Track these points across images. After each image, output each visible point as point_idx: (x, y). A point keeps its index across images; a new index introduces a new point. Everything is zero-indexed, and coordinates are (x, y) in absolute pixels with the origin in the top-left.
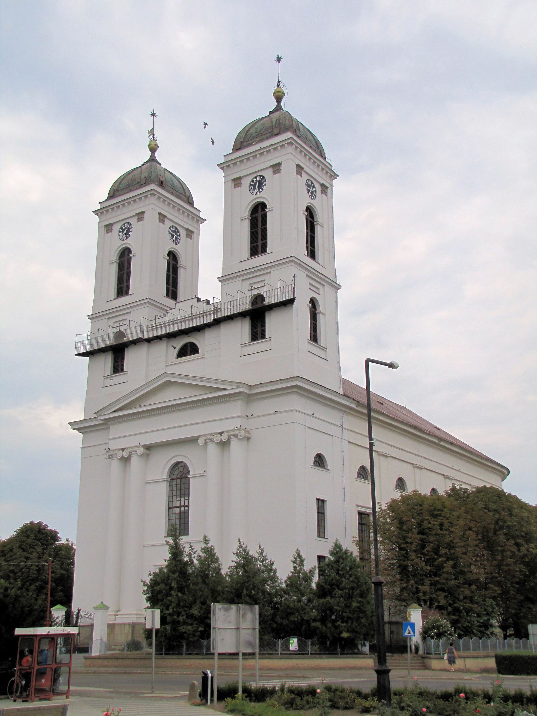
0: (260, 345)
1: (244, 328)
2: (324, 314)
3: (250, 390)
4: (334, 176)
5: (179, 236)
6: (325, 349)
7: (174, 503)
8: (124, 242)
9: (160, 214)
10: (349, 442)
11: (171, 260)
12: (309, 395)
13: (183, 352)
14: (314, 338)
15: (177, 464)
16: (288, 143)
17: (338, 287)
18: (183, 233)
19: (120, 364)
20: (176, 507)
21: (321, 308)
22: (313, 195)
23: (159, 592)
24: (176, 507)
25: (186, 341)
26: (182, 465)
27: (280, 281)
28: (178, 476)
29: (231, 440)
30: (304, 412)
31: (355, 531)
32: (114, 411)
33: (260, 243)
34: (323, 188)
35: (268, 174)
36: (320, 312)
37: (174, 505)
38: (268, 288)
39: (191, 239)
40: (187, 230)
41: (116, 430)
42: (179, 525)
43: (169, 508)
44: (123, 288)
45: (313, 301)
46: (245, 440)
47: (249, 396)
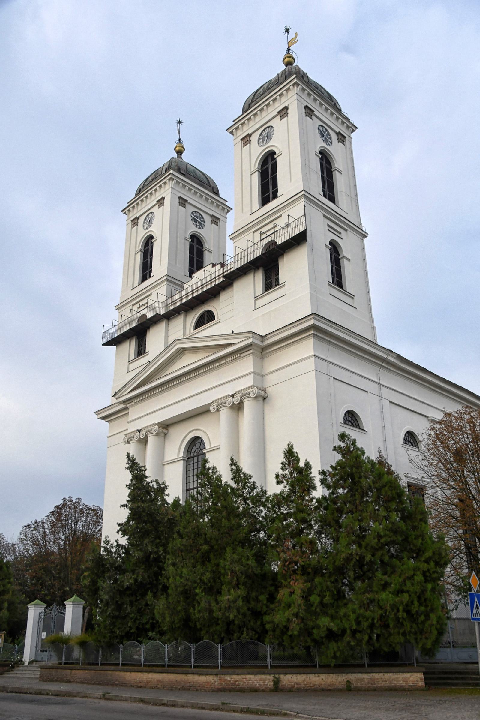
0: (275, 294)
1: (256, 280)
2: (349, 260)
3: (262, 342)
4: (353, 128)
5: (204, 221)
6: (352, 296)
7: (192, 484)
8: (147, 231)
9: (180, 198)
10: (390, 402)
11: (195, 244)
12: (331, 340)
13: (199, 323)
14: (338, 280)
16: (293, 85)
17: (364, 236)
18: (208, 219)
19: (143, 348)
20: (193, 489)
24: (193, 489)
25: (200, 307)
26: (199, 441)
27: (290, 217)
28: (196, 454)
29: (244, 401)
30: (327, 359)
34: (340, 137)
36: (344, 257)
37: (192, 487)
39: (217, 225)
40: (212, 216)
41: (135, 411)
43: (187, 490)
44: (146, 272)
46: (261, 399)
47: (264, 349)
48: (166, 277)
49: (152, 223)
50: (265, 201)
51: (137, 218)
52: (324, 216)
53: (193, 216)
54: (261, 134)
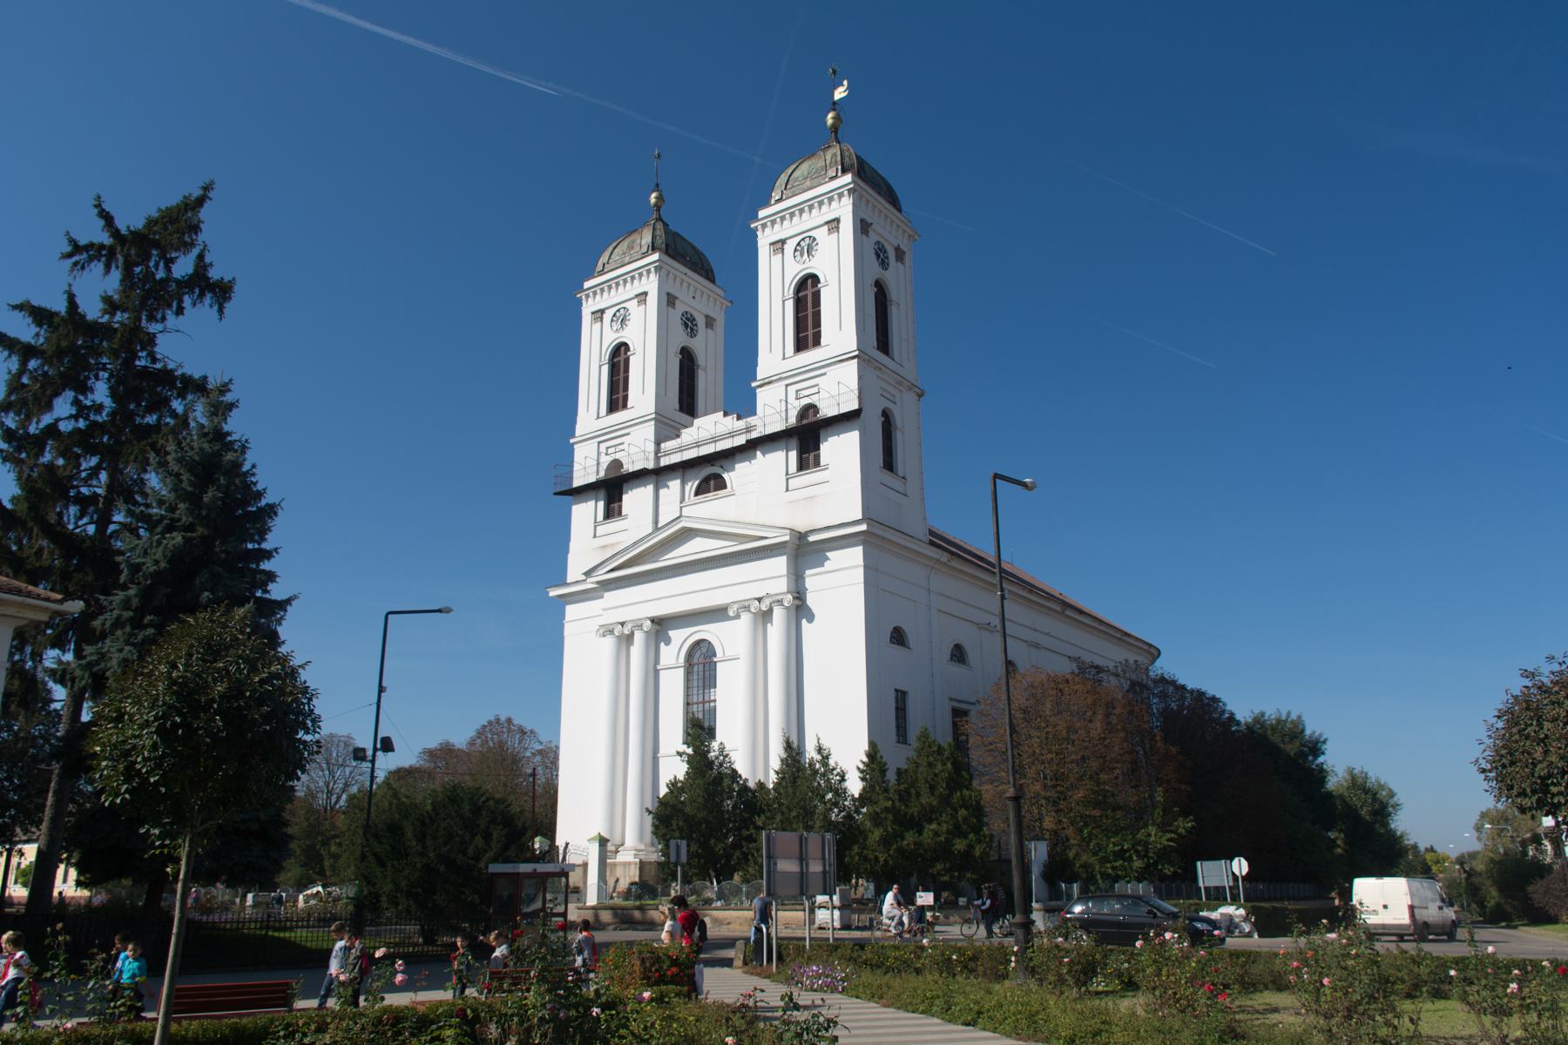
15: (698, 643)
21: (898, 420)
22: (884, 264)
23: (669, 816)
25: (709, 472)
31: (950, 739)
32: (612, 570)
33: (810, 332)
35: (821, 234)
38: (823, 394)
42: (699, 730)
45: (886, 414)
50: (801, 346)
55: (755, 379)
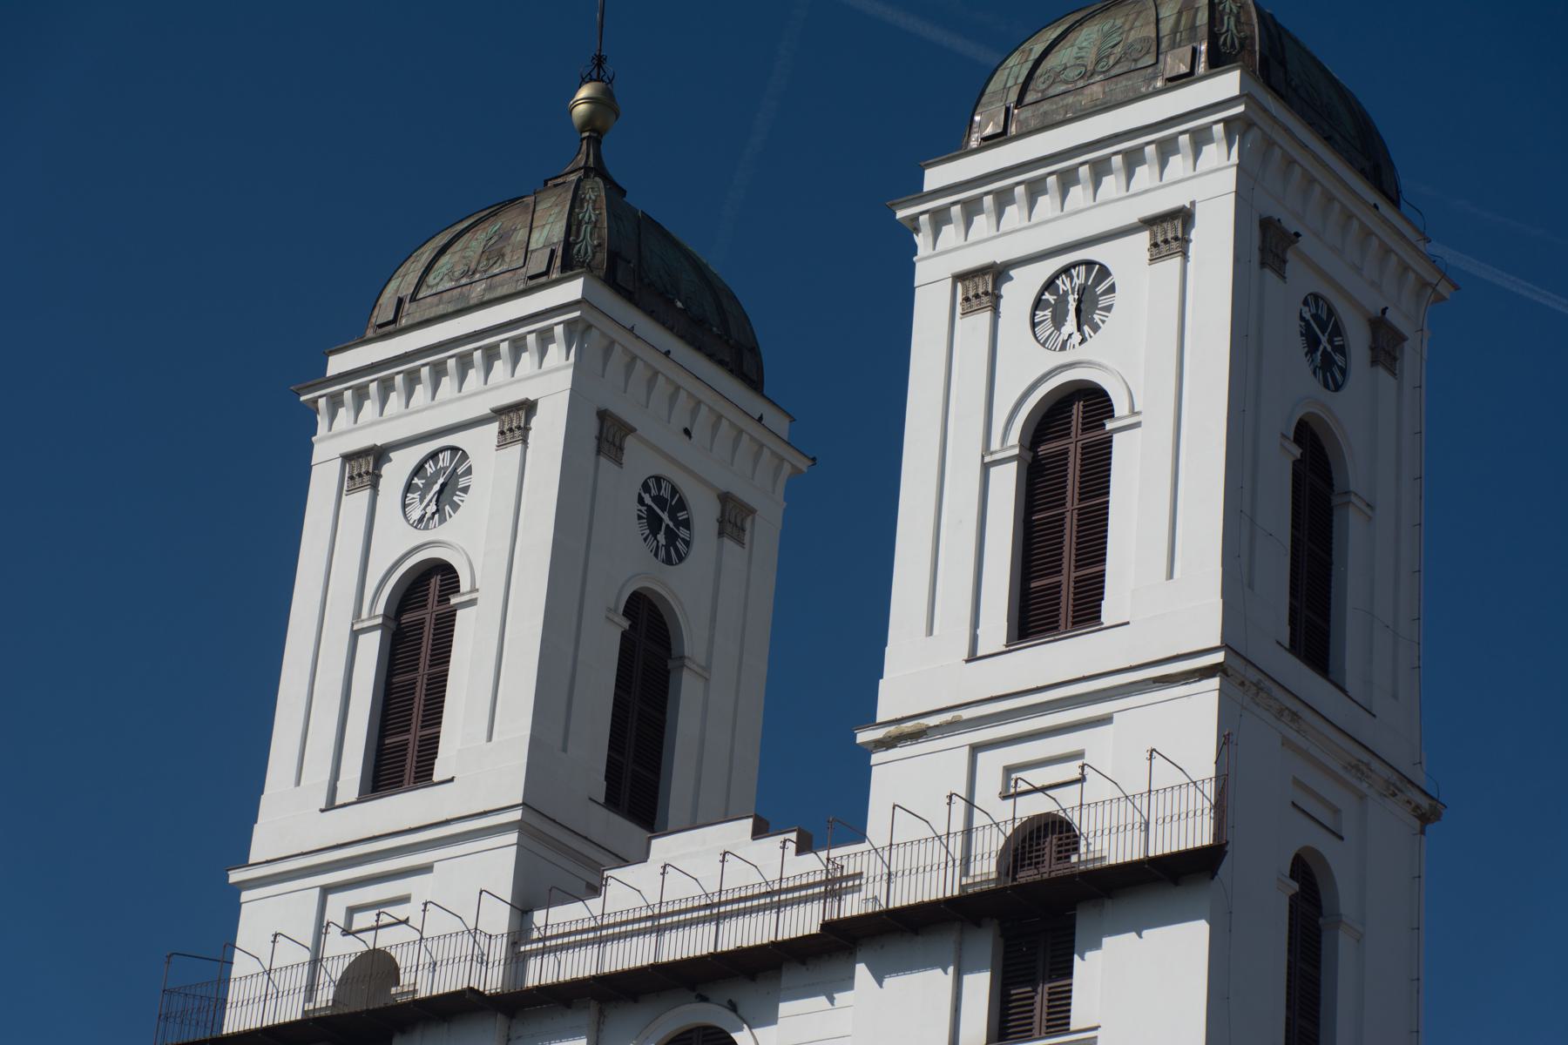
8: (422, 536)
27: (1158, 760)
48: (516, 815)
49: (455, 507)
50: (1034, 618)
51: (379, 455)
52: (1286, 742)
53: (648, 500)
54: (1050, 285)
55: (243, 861)
